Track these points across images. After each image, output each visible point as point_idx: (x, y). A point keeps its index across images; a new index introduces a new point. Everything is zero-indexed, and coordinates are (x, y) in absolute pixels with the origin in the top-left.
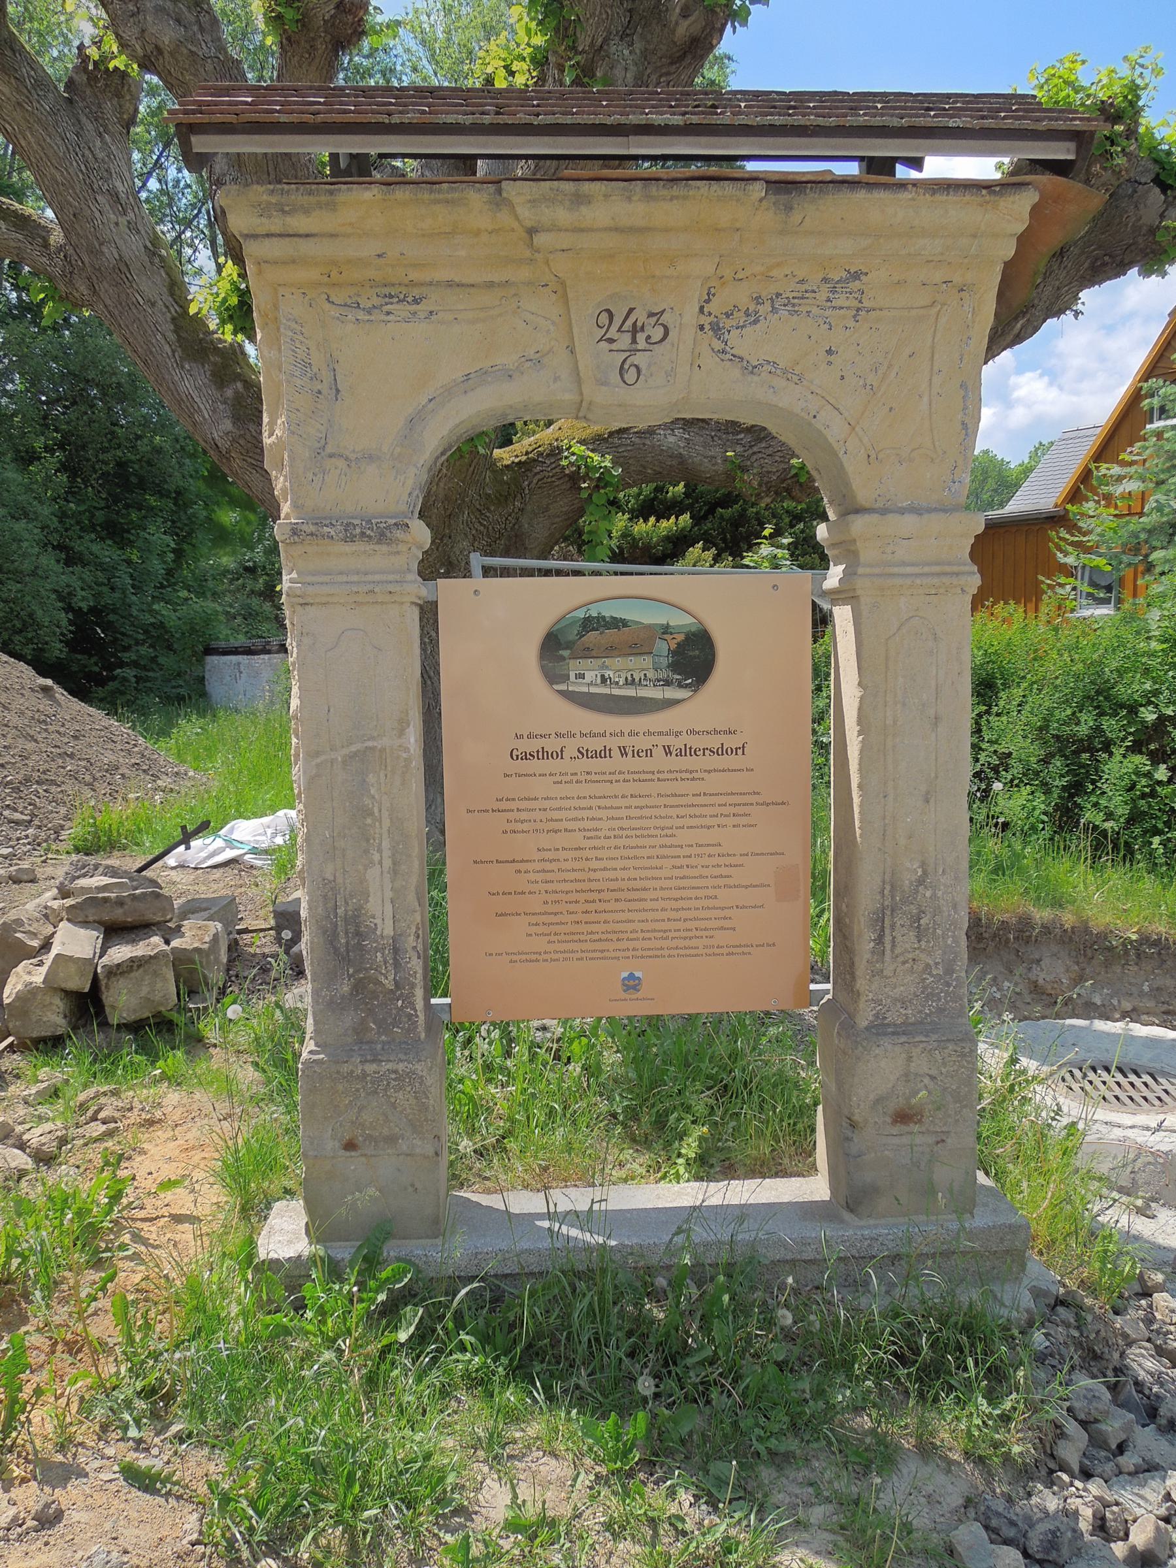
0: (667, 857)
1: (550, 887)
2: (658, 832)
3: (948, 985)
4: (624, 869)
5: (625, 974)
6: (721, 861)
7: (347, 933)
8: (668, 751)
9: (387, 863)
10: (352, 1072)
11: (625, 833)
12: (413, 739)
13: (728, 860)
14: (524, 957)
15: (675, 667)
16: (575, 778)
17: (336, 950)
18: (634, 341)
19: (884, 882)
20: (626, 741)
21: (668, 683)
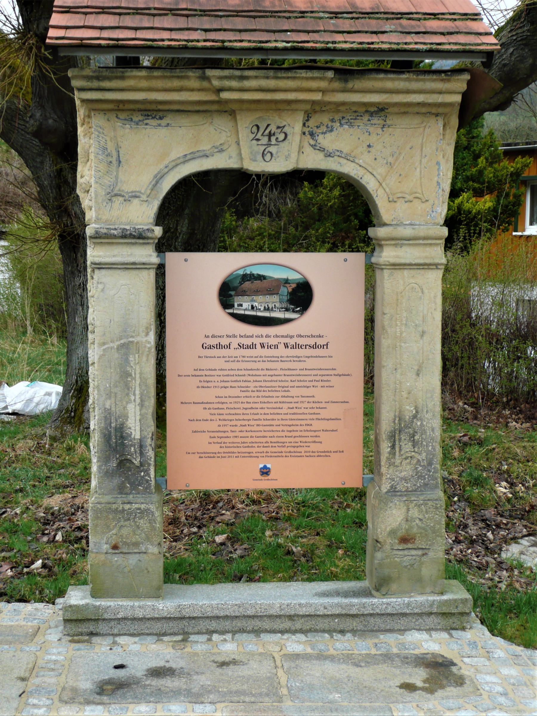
0: (286, 402)
1: (221, 417)
2: (280, 389)
3: (430, 471)
4: (262, 408)
5: (261, 466)
6: (315, 405)
7: (116, 436)
8: (262, 346)
9: (138, 401)
10: (117, 508)
11: (262, 389)
12: (152, 338)
13: (318, 405)
14: (207, 455)
15: (291, 301)
16: (236, 359)
17: (110, 445)
18: (270, 140)
19: (395, 416)
20: (264, 340)
21: (287, 310)
